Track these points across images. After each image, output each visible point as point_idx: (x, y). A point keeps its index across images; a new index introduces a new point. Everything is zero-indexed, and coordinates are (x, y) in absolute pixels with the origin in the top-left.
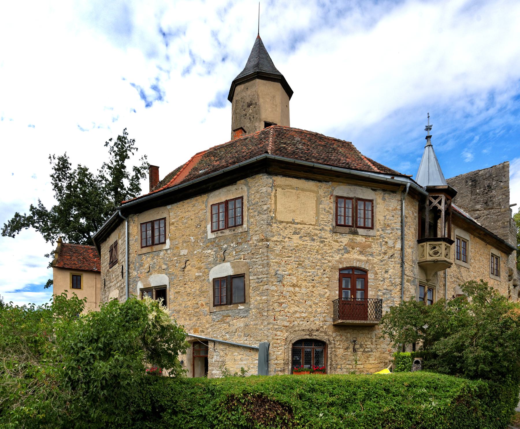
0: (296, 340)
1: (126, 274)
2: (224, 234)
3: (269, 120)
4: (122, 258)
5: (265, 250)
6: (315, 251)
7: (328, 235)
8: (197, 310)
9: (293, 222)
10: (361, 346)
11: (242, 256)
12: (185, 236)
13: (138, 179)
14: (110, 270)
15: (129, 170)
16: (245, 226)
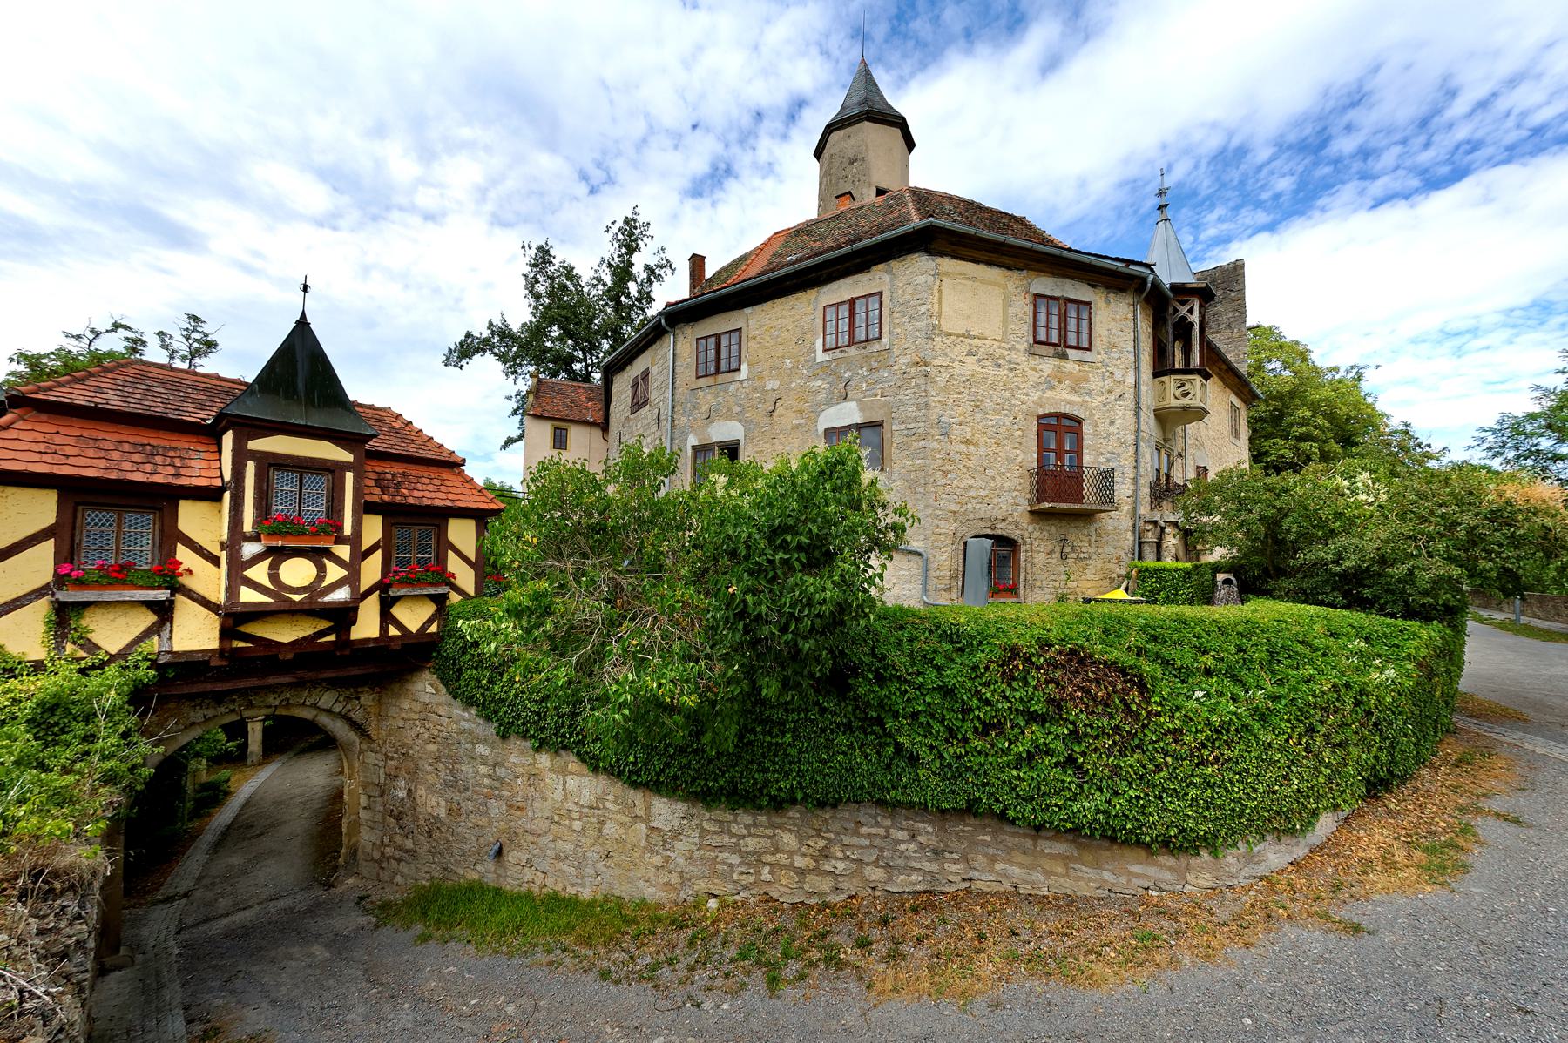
3: (883, 186)
5: (922, 380)
7: (1021, 358)
9: (967, 336)
10: (1073, 548)
13: (651, 282)
15: (638, 269)
16: (885, 340)
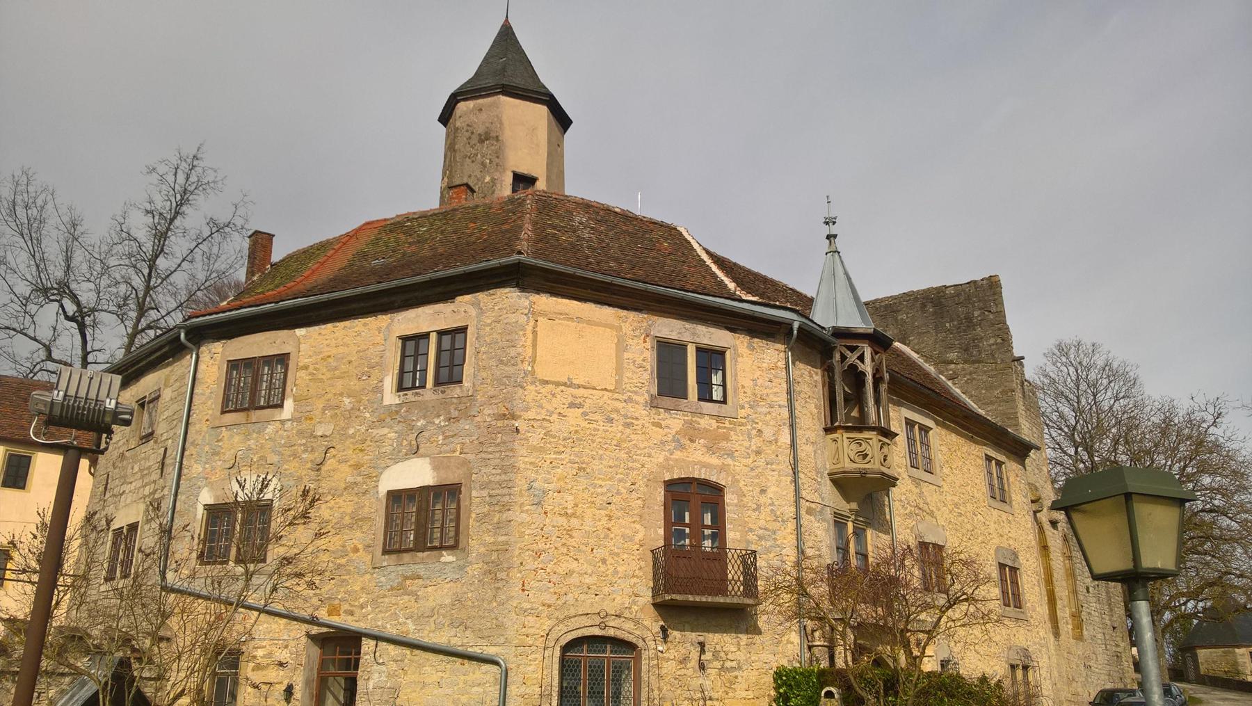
3: (523, 170)
6: (615, 442)
7: (641, 412)
8: (343, 561)
9: (569, 384)
10: (716, 655)
11: (458, 447)
12: (330, 396)
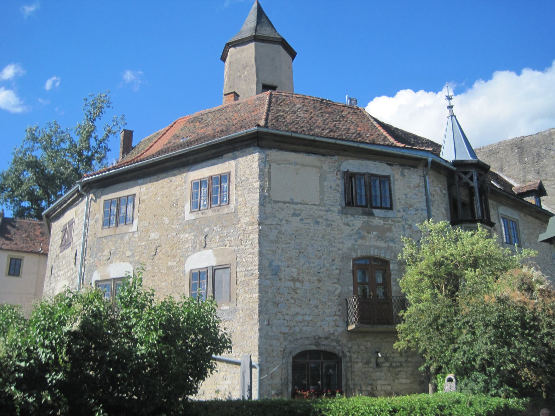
0: (298, 351)
1: (79, 262)
2: (206, 215)
3: (269, 82)
4: (77, 240)
6: (321, 236)
7: (335, 216)
9: (292, 202)
14: (60, 255)
16: (232, 205)
